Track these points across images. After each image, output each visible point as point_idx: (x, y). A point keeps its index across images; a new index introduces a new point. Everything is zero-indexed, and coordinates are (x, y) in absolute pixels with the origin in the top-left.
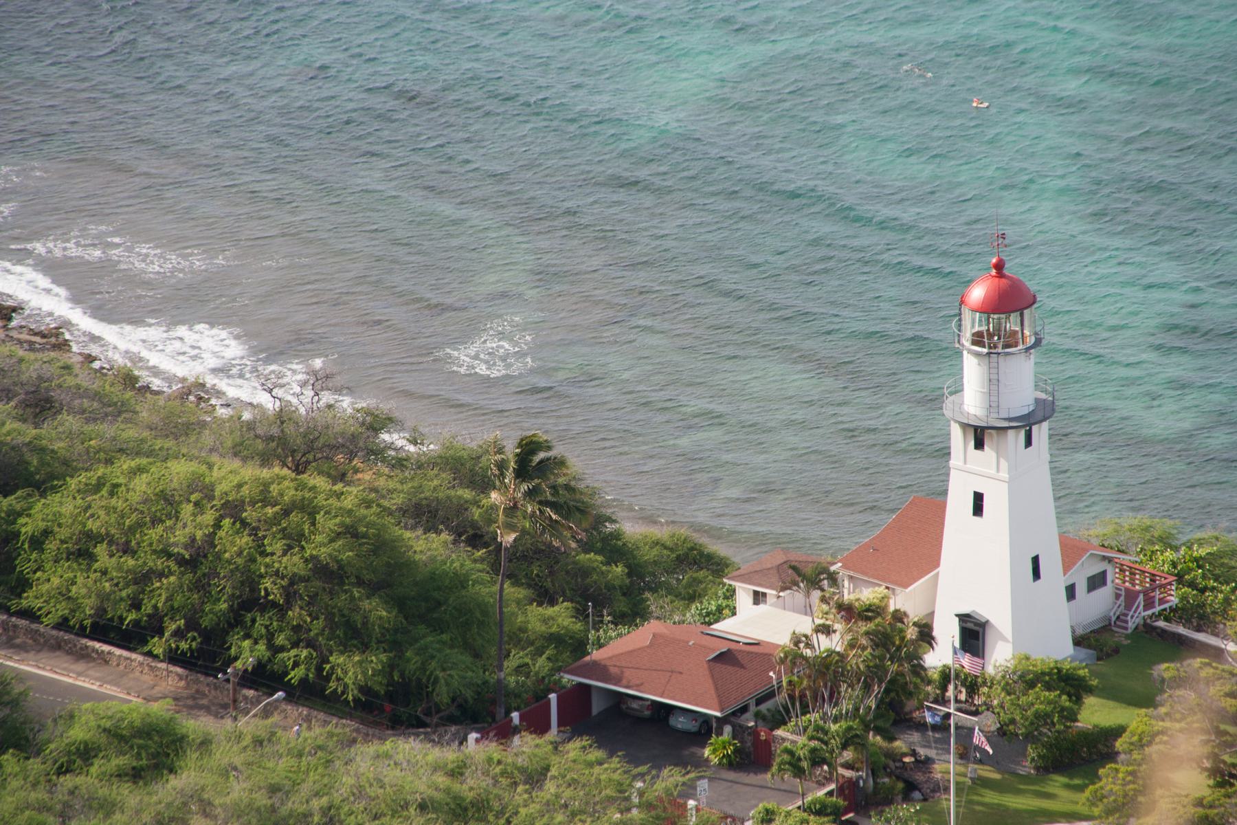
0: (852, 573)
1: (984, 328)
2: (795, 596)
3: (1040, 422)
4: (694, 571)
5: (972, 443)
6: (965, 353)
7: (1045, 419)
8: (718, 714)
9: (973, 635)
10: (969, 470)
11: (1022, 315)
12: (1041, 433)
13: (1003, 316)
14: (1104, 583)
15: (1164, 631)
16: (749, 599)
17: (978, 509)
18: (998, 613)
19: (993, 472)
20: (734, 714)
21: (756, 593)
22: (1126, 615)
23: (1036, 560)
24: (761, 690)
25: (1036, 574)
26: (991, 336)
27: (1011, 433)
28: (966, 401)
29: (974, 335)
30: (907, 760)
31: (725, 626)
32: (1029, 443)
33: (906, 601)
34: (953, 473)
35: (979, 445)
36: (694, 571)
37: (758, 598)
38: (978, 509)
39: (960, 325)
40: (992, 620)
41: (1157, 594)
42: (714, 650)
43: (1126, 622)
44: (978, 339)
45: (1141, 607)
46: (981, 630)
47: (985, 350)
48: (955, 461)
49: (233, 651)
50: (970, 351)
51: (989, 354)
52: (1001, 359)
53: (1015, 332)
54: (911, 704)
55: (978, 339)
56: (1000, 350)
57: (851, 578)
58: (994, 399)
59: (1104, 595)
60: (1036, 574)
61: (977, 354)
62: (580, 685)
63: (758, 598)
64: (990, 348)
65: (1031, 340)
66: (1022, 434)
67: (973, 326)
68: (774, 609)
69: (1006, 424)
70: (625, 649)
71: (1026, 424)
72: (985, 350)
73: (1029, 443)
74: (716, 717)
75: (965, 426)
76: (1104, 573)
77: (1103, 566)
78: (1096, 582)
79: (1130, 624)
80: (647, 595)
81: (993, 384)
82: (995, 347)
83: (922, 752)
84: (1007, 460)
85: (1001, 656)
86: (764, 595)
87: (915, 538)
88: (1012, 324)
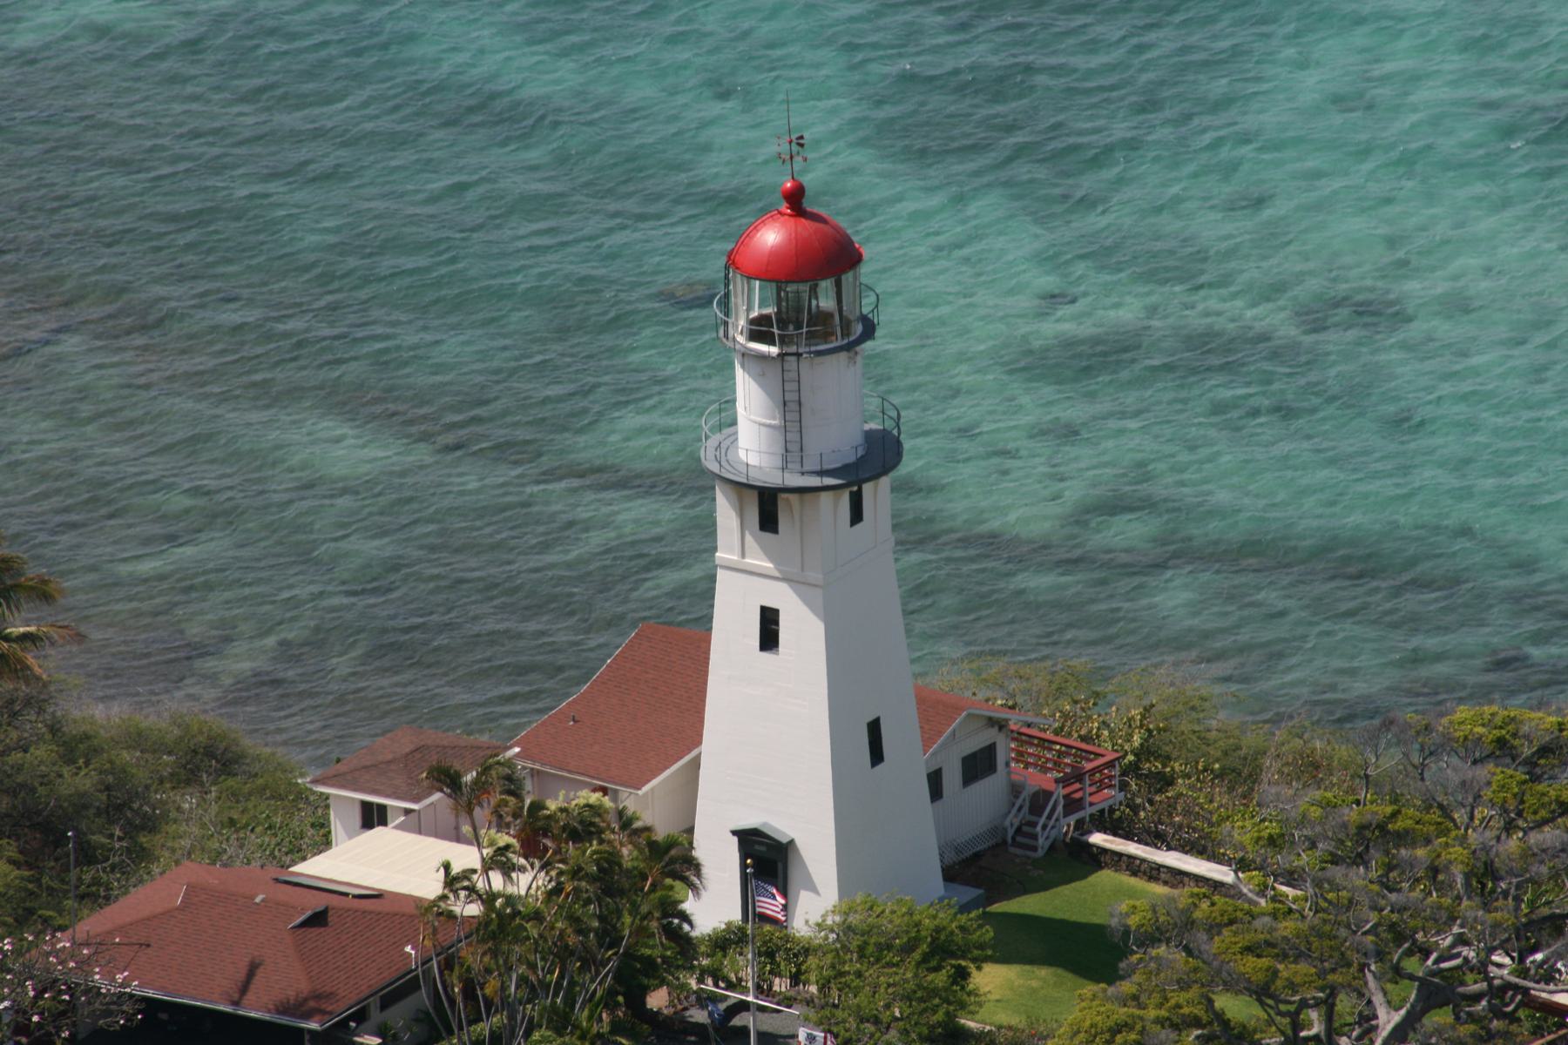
1: (770, 310)
9: (766, 859)
11: (838, 285)
17: (769, 638)
21: (367, 807)
22: (1034, 825)
23: (874, 728)
25: (877, 755)
27: (825, 497)
29: (753, 322)
31: (315, 867)
32: (857, 516)
33: (648, 803)
35: (768, 522)
37: (372, 817)
38: (769, 638)
43: (1035, 837)
44: (760, 329)
45: (1060, 809)
47: (774, 350)
48: (725, 553)
51: (781, 356)
59: (991, 788)
60: (877, 755)
67: (749, 310)
69: (814, 481)
73: (857, 516)
76: (990, 750)
78: (978, 765)
79: (1041, 841)
81: (791, 410)
85: (813, 908)
86: (382, 809)
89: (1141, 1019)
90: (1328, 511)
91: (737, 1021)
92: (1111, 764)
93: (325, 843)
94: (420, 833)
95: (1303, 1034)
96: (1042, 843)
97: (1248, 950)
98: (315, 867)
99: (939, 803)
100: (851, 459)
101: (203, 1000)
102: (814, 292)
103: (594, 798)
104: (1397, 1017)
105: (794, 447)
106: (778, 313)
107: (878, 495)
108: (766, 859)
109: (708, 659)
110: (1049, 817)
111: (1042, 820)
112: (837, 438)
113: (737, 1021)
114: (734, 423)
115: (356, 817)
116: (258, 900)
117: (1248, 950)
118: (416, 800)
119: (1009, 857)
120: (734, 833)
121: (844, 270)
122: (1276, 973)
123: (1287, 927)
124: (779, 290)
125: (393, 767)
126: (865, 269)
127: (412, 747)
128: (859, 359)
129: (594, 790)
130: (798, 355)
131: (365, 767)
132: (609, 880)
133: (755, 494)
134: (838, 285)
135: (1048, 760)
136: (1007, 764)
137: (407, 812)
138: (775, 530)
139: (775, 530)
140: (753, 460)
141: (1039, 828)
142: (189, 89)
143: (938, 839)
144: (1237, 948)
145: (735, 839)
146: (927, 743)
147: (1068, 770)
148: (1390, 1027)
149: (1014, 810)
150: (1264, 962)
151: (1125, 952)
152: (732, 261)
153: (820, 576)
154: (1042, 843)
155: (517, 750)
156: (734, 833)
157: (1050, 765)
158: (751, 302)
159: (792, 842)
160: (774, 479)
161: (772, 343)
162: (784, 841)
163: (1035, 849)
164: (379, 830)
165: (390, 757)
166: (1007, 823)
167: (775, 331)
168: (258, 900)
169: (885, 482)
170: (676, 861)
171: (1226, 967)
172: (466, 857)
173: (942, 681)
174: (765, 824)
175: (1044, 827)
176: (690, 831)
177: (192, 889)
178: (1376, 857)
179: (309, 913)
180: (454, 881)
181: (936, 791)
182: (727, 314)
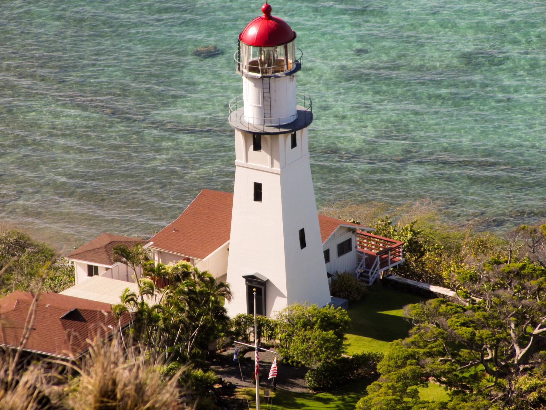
0: (160, 250)
1: (257, 58)
2: (119, 267)
5: (252, 147)
6: (244, 78)
9: (258, 289)
10: (251, 167)
11: (286, 48)
13: (271, 49)
14: (350, 249)
16: (85, 273)
17: (258, 196)
18: (276, 274)
19: (268, 167)
22: (368, 272)
23: (302, 233)
25: (303, 244)
26: (263, 64)
27: (281, 137)
29: (250, 63)
30: (217, 386)
31: (68, 292)
32: (294, 144)
33: (206, 265)
34: (238, 169)
37: (92, 271)
38: (258, 196)
39: (239, 57)
40: (272, 280)
43: (368, 277)
44: (253, 67)
45: (378, 266)
46: (263, 288)
47: (259, 75)
48: (240, 160)
49: (162, 290)
50: (248, 77)
51: (263, 78)
52: (272, 80)
53: (283, 61)
54: (34, 362)
55: (253, 67)
56: (271, 74)
57: (160, 253)
59: (349, 257)
60: (303, 244)
61: (253, 79)
63: (92, 271)
64: (263, 73)
65: (291, 67)
66: (289, 137)
67: (249, 58)
68: (103, 278)
69: (277, 130)
72: (259, 75)
73: (294, 144)
75: (246, 133)
76: (349, 241)
77: (349, 235)
78: (344, 248)
79: (371, 279)
81: (267, 102)
82: (266, 72)
83: (226, 379)
84: (278, 160)
85: (278, 308)
86: (96, 268)
87: (213, 221)
88: (279, 52)
89: (418, 353)
91: (247, 356)
92: (398, 247)
94: (119, 279)
95: (485, 359)
96: (371, 279)
97: (463, 325)
98: (68, 292)
99: (328, 263)
100: (292, 120)
101: (186, 255)
103: (184, 262)
104: (524, 351)
105: (268, 116)
107: (303, 135)
108: (258, 289)
109: (232, 204)
110: (374, 269)
111: (371, 270)
112: (286, 113)
113: (247, 356)
114: (242, 104)
116: (47, 306)
117: (463, 325)
119: (372, 289)
120: (244, 277)
122: (474, 334)
123: (478, 315)
125: (101, 250)
127: (108, 242)
128: (295, 79)
129: (184, 259)
131: (88, 251)
132: (195, 299)
133: (252, 135)
134: (286, 48)
135: (372, 245)
136: (356, 247)
137: (107, 269)
140: (251, 121)
141: (370, 274)
144: (458, 324)
145: (244, 280)
146: (324, 238)
147: (381, 249)
148: (521, 355)
149: (359, 266)
150: (471, 329)
151: (411, 326)
152: (241, 38)
153: (280, 170)
154: (371, 279)
155: (152, 243)
156: (244, 277)
157: (373, 247)
158: (249, 55)
160: (259, 129)
161: (258, 72)
162: (265, 280)
163: (368, 282)
164: (95, 277)
165: (99, 246)
166: (356, 272)
167: (260, 67)
168: (47, 306)
169: (305, 130)
171: (27, 242)
172: (134, 288)
173: (331, 211)
174: (257, 273)
175: (372, 273)
176: (225, 276)
178: (515, 283)
179: (69, 312)
181: (327, 259)
182: (239, 60)
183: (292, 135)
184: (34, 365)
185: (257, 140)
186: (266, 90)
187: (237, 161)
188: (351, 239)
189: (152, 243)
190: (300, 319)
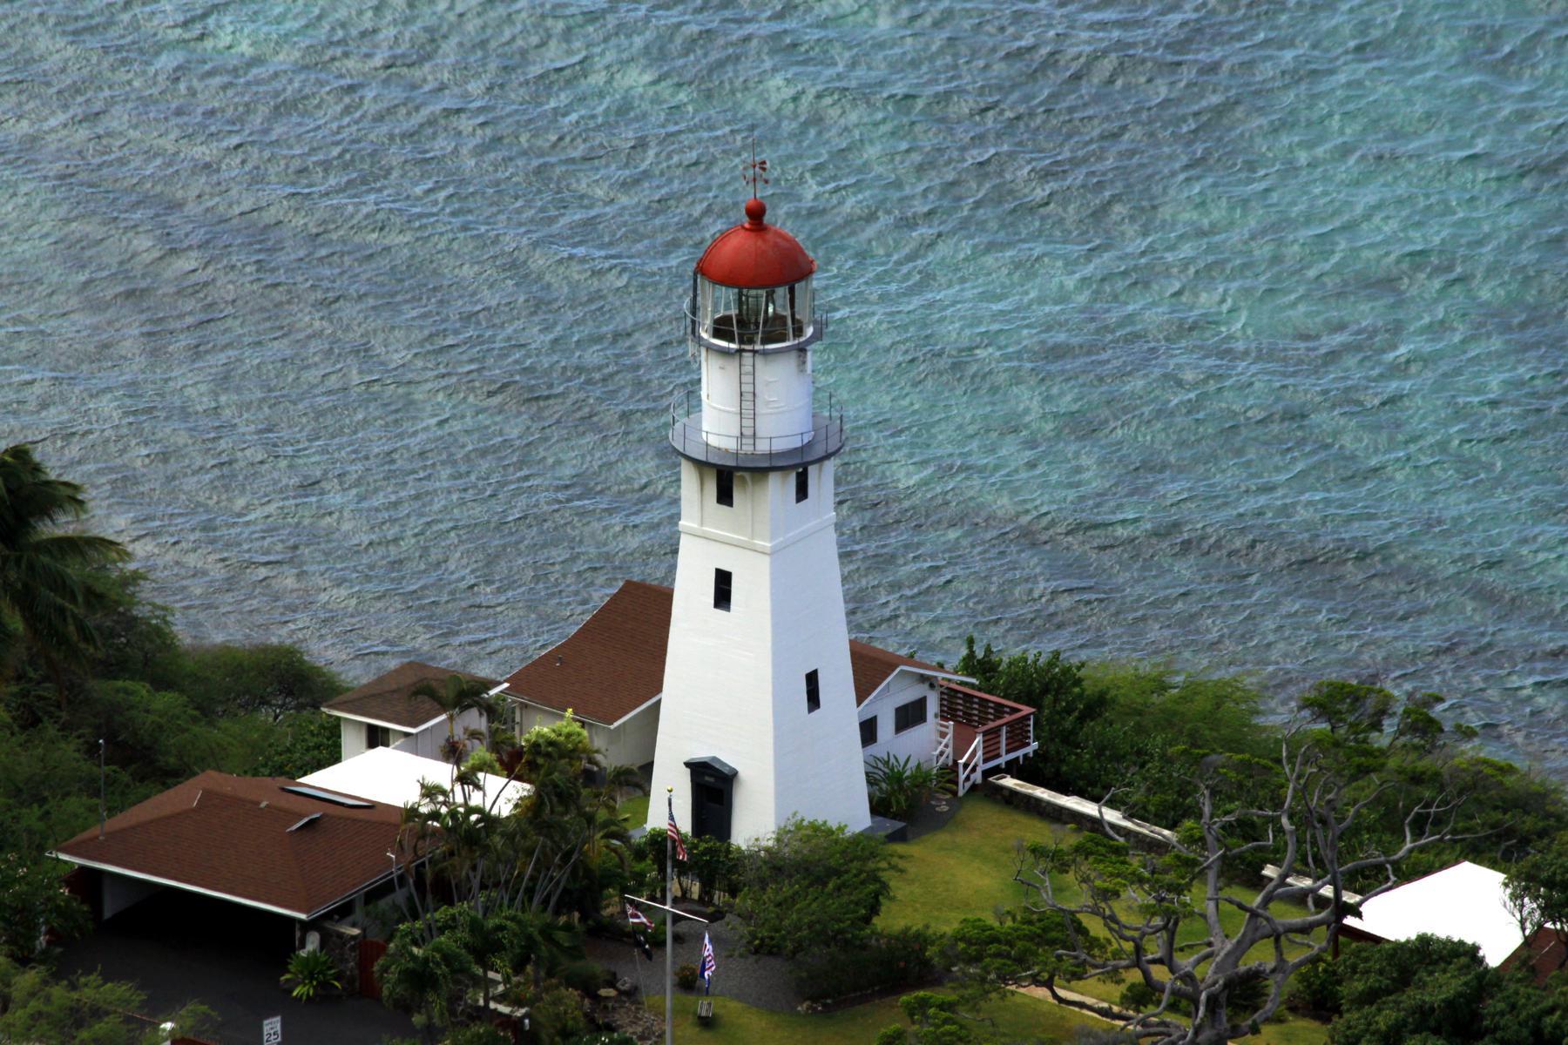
3: (820, 460)
4: (295, 703)
7: (827, 457)
8: (303, 916)
10: (705, 539)
11: (792, 291)
12: (822, 482)
13: (763, 292)
15: (1013, 793)
20: (328, 916)
21: (372, 729)
23: (812, 679)
24: (376, 880)
25: (813, 700)
28: (705, 427)
31: (323, 780)
32: (802, 492)
34: (685, 544)
35: (725, 497)
36: (295, 703)
37: (376, 738)
41: (1326, 43)
42: (301, 817)
47: (733, 346)
56: (758, 347)
58: (748, 423)
60: (813, 700)
62: (83, 868)
67: (715, 310)
70: (167, 811)
71: (798, 469)
73: (802, 492)
74: (301, 921)
80: (878, 922)
81: (747, 398)
90: (1393, 386)
93: (335, 758)
102: (770, 298)
105: (748, 413)
106: (740, 314)
115: (363, 738)
116: (263, 805)
118: (414, 726)
120: (687, 764)
121: (799, 280)
124: (740, 295)
126: (816, 282)
130: (755, 352)
138: (730, 504)
139: (730, 504)
142: (393, 407)
143: (777, 818)
156: (687, 764)
159: (735, 774)
161: (732, 340)
164: (380, 749)
165: (394, 687)
168: (263, 805)
170: (638, 778)
174: (715, 759)
177: (208, 795)
180: (430, 792)
183: (798, 475)
184: (1164, 688)
185: (726, 480)
186: (747, 379)
187: (683, 523)
188: (875, 718)
189: (506, 685)
190: (322, 86)
